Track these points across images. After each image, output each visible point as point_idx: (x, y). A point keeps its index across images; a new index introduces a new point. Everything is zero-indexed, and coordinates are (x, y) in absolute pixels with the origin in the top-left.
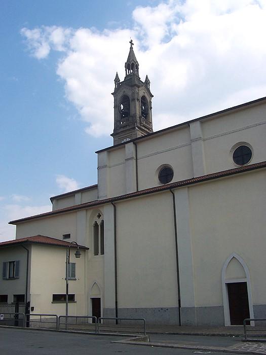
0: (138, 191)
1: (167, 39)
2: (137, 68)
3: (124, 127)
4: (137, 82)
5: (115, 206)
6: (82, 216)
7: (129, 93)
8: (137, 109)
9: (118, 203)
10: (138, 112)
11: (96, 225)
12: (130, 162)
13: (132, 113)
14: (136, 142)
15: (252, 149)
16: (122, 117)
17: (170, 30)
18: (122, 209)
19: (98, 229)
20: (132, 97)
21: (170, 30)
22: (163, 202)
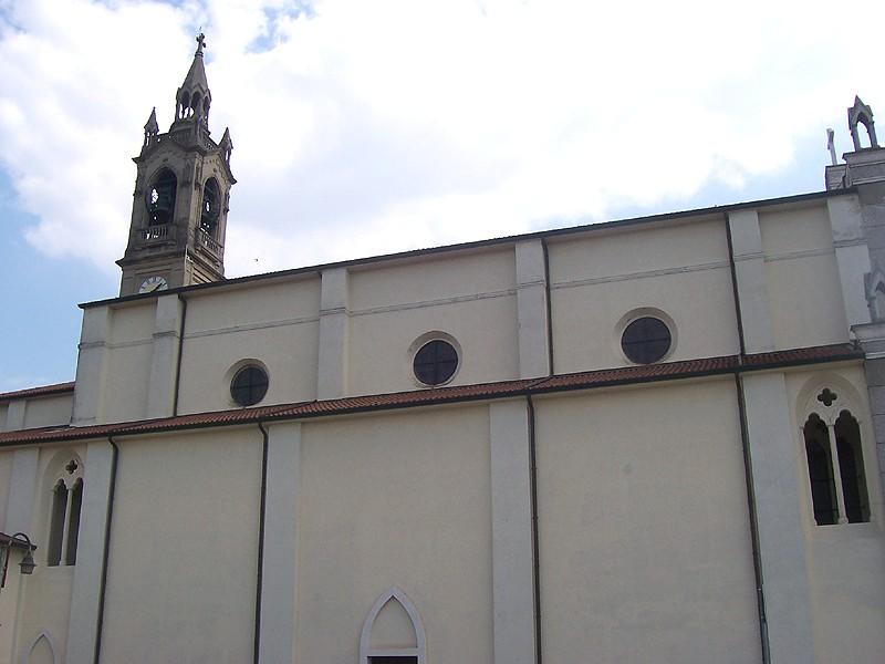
0: (175, 416)
1: (263, 44)
2: (207, 107)
3: (153, 247)
4: (200, 142)
5: (264, 432)
6: (27, 460)
8: (192, 206)
9: (125, 440)
10: (194, 218)
11: (61, 490)
13: (179, 215)
14: (185, 295)
15: (461, 351)
16: (151, 222)
17: (272, 30)
18: (135, 457)
19: (67, 501)
20: (181, 179)
21: (272, 30)
22: (240, 450)
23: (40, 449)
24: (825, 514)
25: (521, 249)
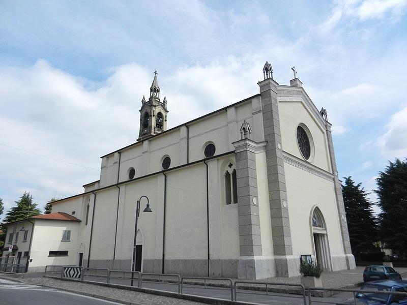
7: (147, 109)
11: (227, 174)
12: (116, 164)
13: (149, 125)
23: (218, 160)
24: (229, 202)
25: (229, 111)
